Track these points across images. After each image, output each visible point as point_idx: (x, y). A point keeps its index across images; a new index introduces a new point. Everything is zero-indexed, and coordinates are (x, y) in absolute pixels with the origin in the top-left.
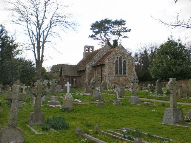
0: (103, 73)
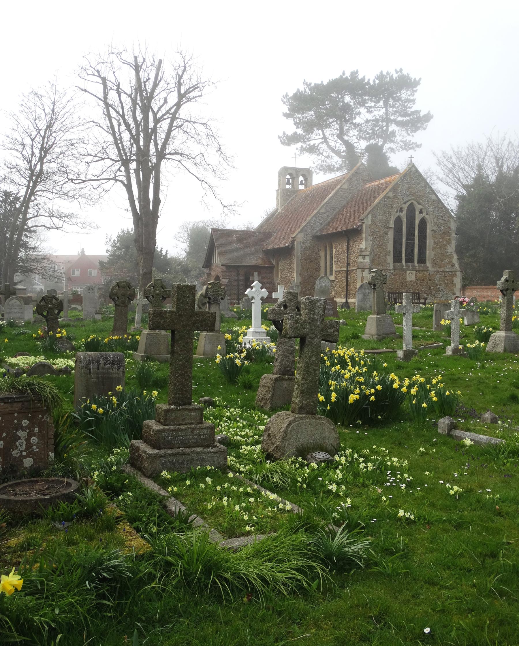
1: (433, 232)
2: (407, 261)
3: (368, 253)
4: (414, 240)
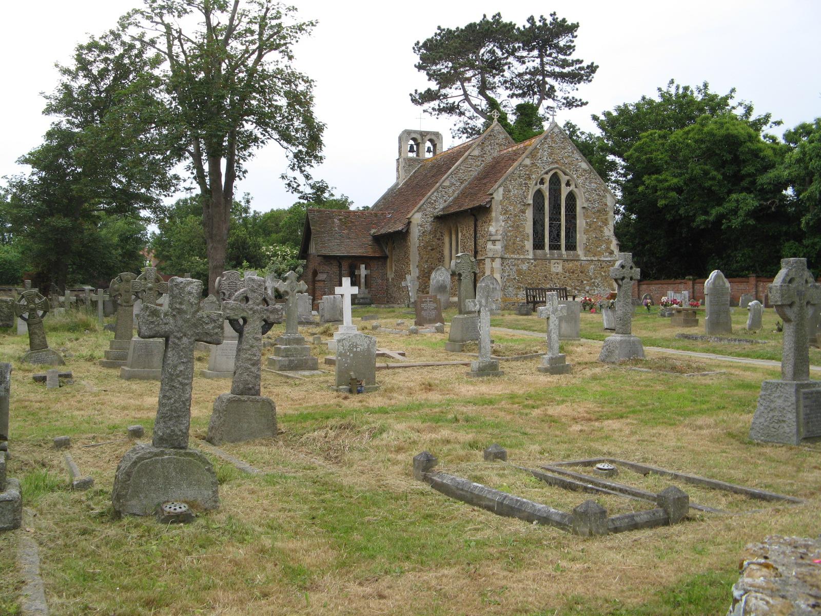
0: (481, 242)
1: (584, 210)
2: (552, 248)
3: (499, 237)
4: (560, 221)
